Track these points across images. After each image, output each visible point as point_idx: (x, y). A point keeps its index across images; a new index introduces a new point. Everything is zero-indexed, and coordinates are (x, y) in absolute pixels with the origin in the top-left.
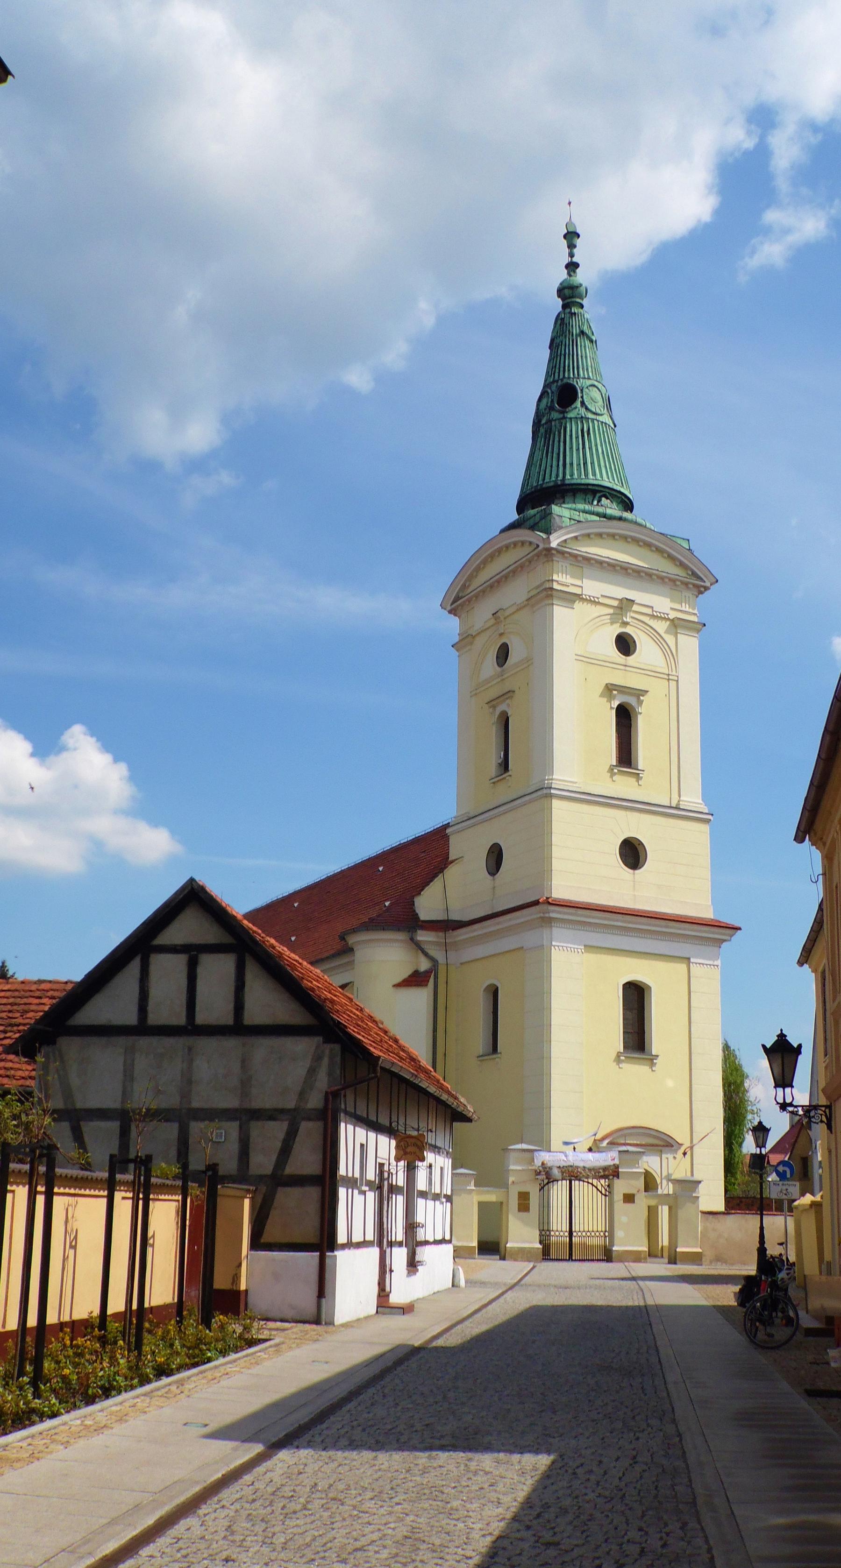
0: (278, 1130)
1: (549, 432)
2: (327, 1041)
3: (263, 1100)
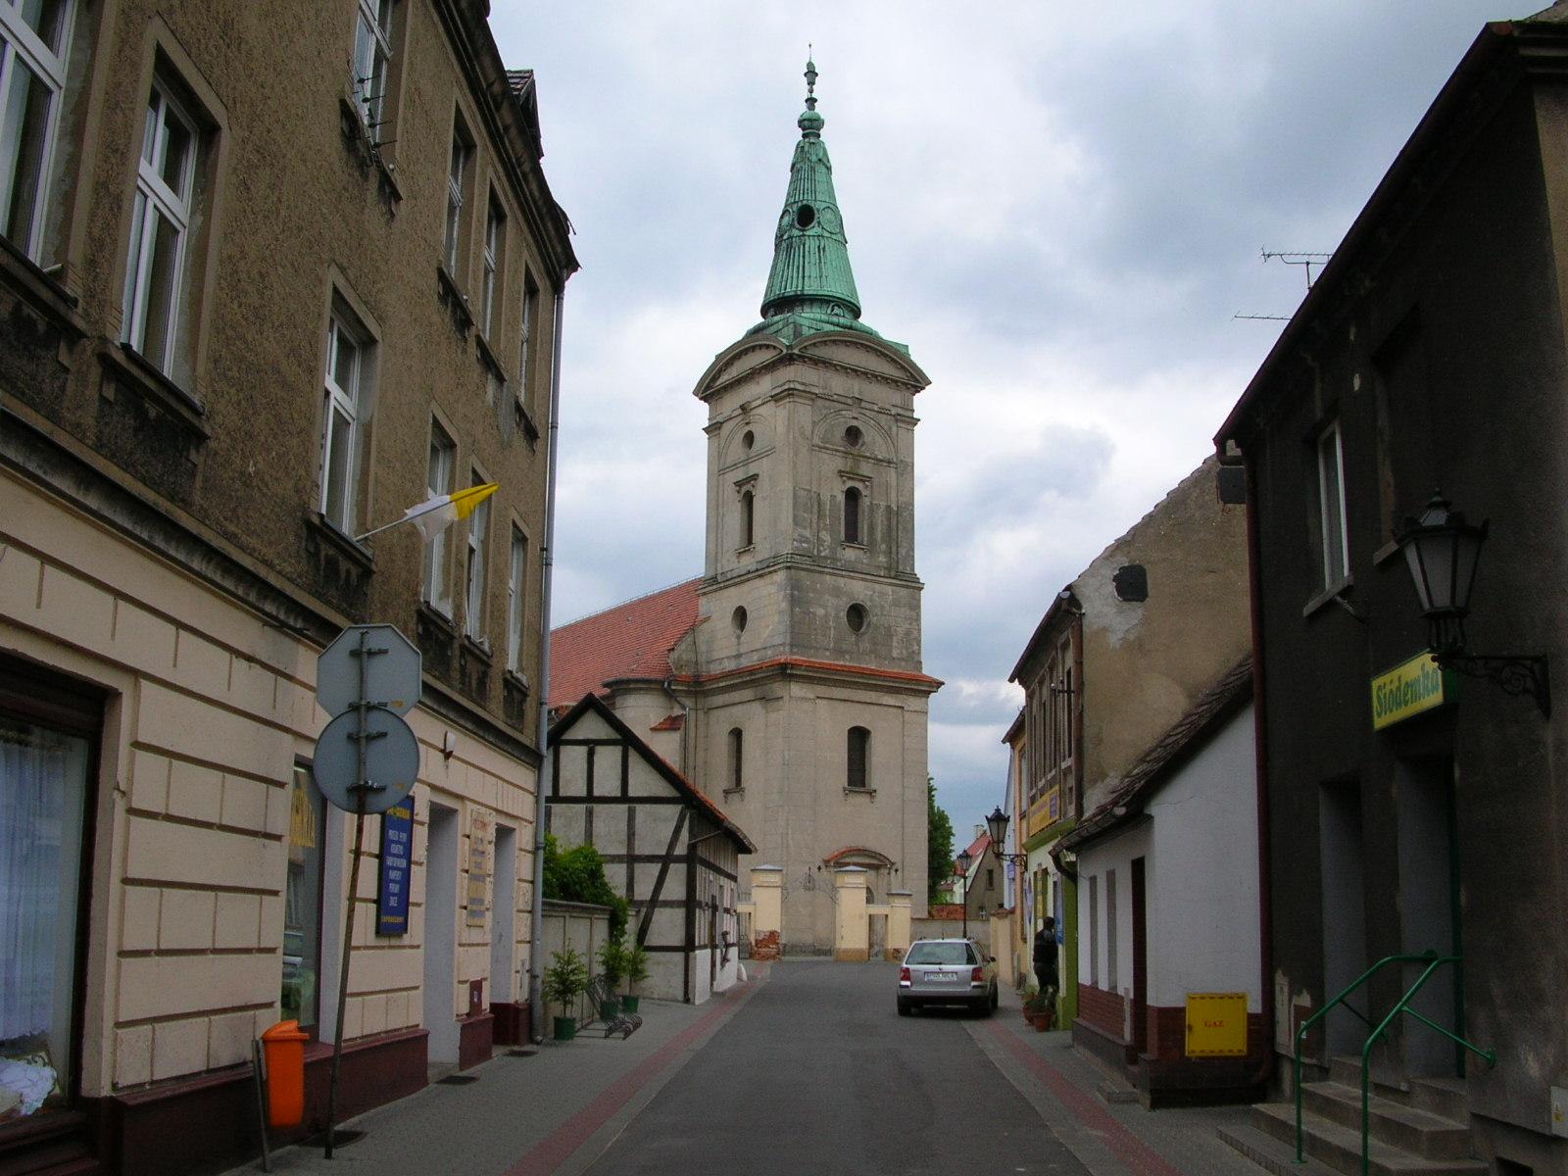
0: (655, 869)
1: (790, 247)
2: (687, 808)
3: (641, 849)
